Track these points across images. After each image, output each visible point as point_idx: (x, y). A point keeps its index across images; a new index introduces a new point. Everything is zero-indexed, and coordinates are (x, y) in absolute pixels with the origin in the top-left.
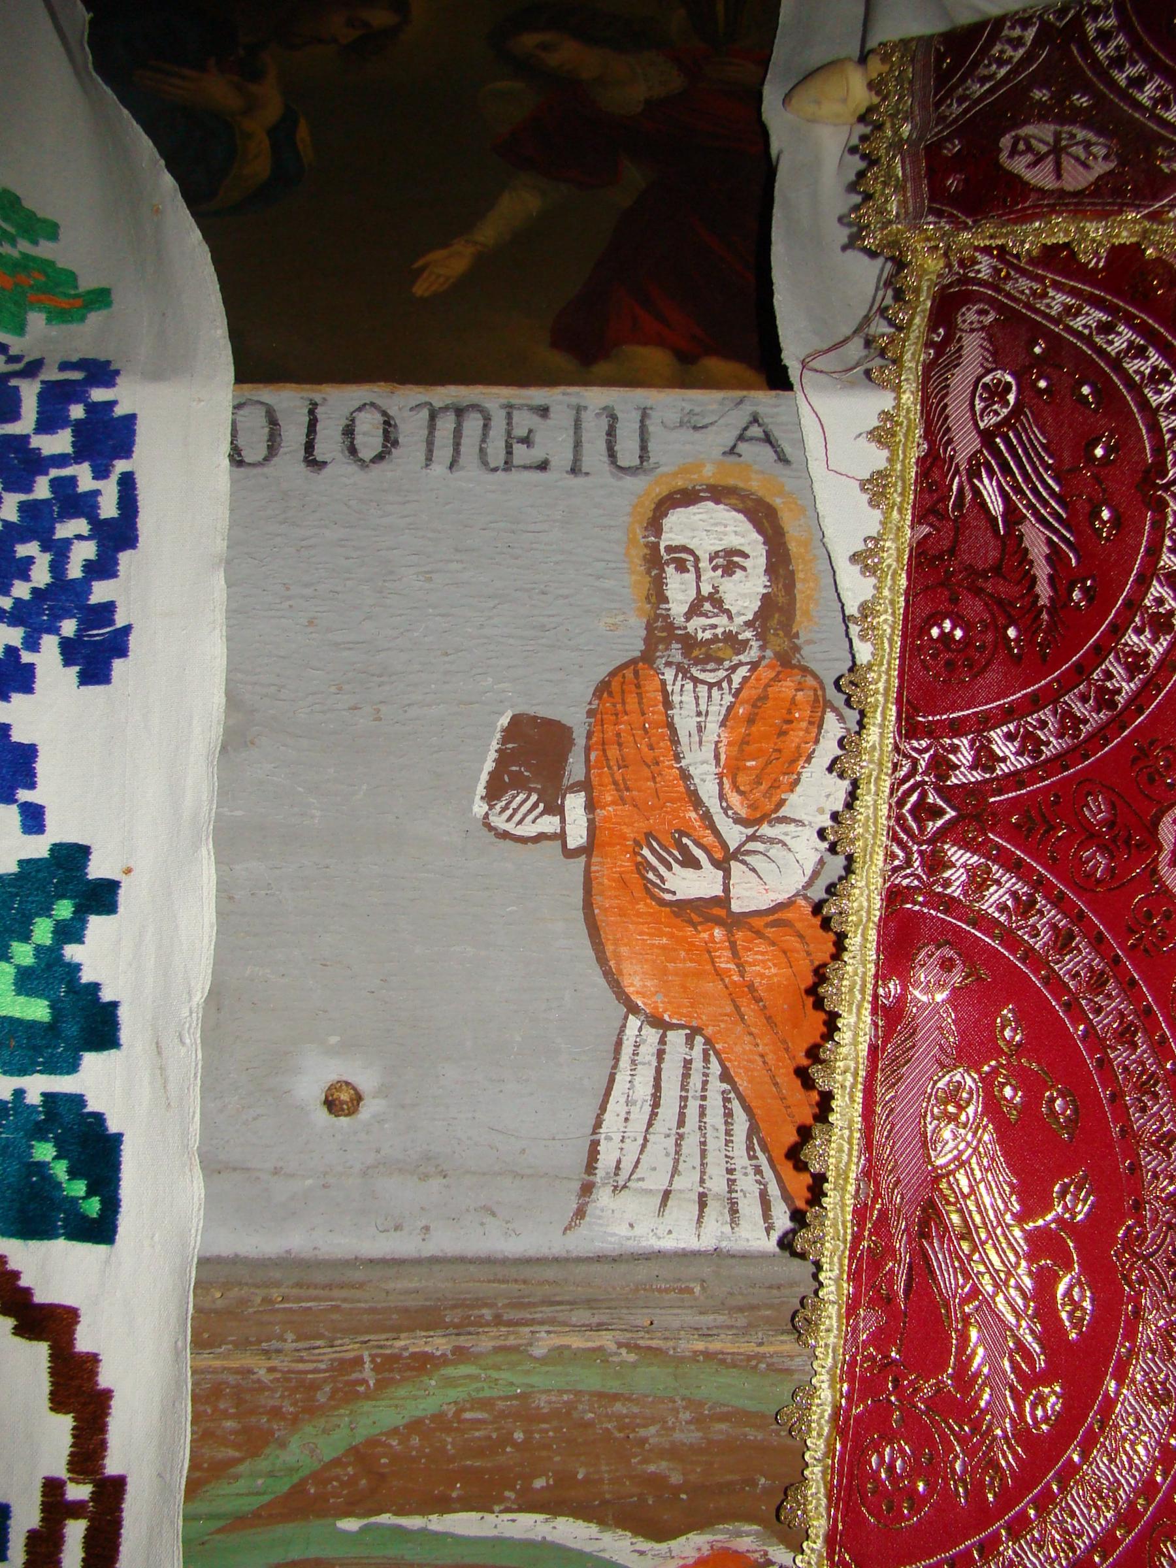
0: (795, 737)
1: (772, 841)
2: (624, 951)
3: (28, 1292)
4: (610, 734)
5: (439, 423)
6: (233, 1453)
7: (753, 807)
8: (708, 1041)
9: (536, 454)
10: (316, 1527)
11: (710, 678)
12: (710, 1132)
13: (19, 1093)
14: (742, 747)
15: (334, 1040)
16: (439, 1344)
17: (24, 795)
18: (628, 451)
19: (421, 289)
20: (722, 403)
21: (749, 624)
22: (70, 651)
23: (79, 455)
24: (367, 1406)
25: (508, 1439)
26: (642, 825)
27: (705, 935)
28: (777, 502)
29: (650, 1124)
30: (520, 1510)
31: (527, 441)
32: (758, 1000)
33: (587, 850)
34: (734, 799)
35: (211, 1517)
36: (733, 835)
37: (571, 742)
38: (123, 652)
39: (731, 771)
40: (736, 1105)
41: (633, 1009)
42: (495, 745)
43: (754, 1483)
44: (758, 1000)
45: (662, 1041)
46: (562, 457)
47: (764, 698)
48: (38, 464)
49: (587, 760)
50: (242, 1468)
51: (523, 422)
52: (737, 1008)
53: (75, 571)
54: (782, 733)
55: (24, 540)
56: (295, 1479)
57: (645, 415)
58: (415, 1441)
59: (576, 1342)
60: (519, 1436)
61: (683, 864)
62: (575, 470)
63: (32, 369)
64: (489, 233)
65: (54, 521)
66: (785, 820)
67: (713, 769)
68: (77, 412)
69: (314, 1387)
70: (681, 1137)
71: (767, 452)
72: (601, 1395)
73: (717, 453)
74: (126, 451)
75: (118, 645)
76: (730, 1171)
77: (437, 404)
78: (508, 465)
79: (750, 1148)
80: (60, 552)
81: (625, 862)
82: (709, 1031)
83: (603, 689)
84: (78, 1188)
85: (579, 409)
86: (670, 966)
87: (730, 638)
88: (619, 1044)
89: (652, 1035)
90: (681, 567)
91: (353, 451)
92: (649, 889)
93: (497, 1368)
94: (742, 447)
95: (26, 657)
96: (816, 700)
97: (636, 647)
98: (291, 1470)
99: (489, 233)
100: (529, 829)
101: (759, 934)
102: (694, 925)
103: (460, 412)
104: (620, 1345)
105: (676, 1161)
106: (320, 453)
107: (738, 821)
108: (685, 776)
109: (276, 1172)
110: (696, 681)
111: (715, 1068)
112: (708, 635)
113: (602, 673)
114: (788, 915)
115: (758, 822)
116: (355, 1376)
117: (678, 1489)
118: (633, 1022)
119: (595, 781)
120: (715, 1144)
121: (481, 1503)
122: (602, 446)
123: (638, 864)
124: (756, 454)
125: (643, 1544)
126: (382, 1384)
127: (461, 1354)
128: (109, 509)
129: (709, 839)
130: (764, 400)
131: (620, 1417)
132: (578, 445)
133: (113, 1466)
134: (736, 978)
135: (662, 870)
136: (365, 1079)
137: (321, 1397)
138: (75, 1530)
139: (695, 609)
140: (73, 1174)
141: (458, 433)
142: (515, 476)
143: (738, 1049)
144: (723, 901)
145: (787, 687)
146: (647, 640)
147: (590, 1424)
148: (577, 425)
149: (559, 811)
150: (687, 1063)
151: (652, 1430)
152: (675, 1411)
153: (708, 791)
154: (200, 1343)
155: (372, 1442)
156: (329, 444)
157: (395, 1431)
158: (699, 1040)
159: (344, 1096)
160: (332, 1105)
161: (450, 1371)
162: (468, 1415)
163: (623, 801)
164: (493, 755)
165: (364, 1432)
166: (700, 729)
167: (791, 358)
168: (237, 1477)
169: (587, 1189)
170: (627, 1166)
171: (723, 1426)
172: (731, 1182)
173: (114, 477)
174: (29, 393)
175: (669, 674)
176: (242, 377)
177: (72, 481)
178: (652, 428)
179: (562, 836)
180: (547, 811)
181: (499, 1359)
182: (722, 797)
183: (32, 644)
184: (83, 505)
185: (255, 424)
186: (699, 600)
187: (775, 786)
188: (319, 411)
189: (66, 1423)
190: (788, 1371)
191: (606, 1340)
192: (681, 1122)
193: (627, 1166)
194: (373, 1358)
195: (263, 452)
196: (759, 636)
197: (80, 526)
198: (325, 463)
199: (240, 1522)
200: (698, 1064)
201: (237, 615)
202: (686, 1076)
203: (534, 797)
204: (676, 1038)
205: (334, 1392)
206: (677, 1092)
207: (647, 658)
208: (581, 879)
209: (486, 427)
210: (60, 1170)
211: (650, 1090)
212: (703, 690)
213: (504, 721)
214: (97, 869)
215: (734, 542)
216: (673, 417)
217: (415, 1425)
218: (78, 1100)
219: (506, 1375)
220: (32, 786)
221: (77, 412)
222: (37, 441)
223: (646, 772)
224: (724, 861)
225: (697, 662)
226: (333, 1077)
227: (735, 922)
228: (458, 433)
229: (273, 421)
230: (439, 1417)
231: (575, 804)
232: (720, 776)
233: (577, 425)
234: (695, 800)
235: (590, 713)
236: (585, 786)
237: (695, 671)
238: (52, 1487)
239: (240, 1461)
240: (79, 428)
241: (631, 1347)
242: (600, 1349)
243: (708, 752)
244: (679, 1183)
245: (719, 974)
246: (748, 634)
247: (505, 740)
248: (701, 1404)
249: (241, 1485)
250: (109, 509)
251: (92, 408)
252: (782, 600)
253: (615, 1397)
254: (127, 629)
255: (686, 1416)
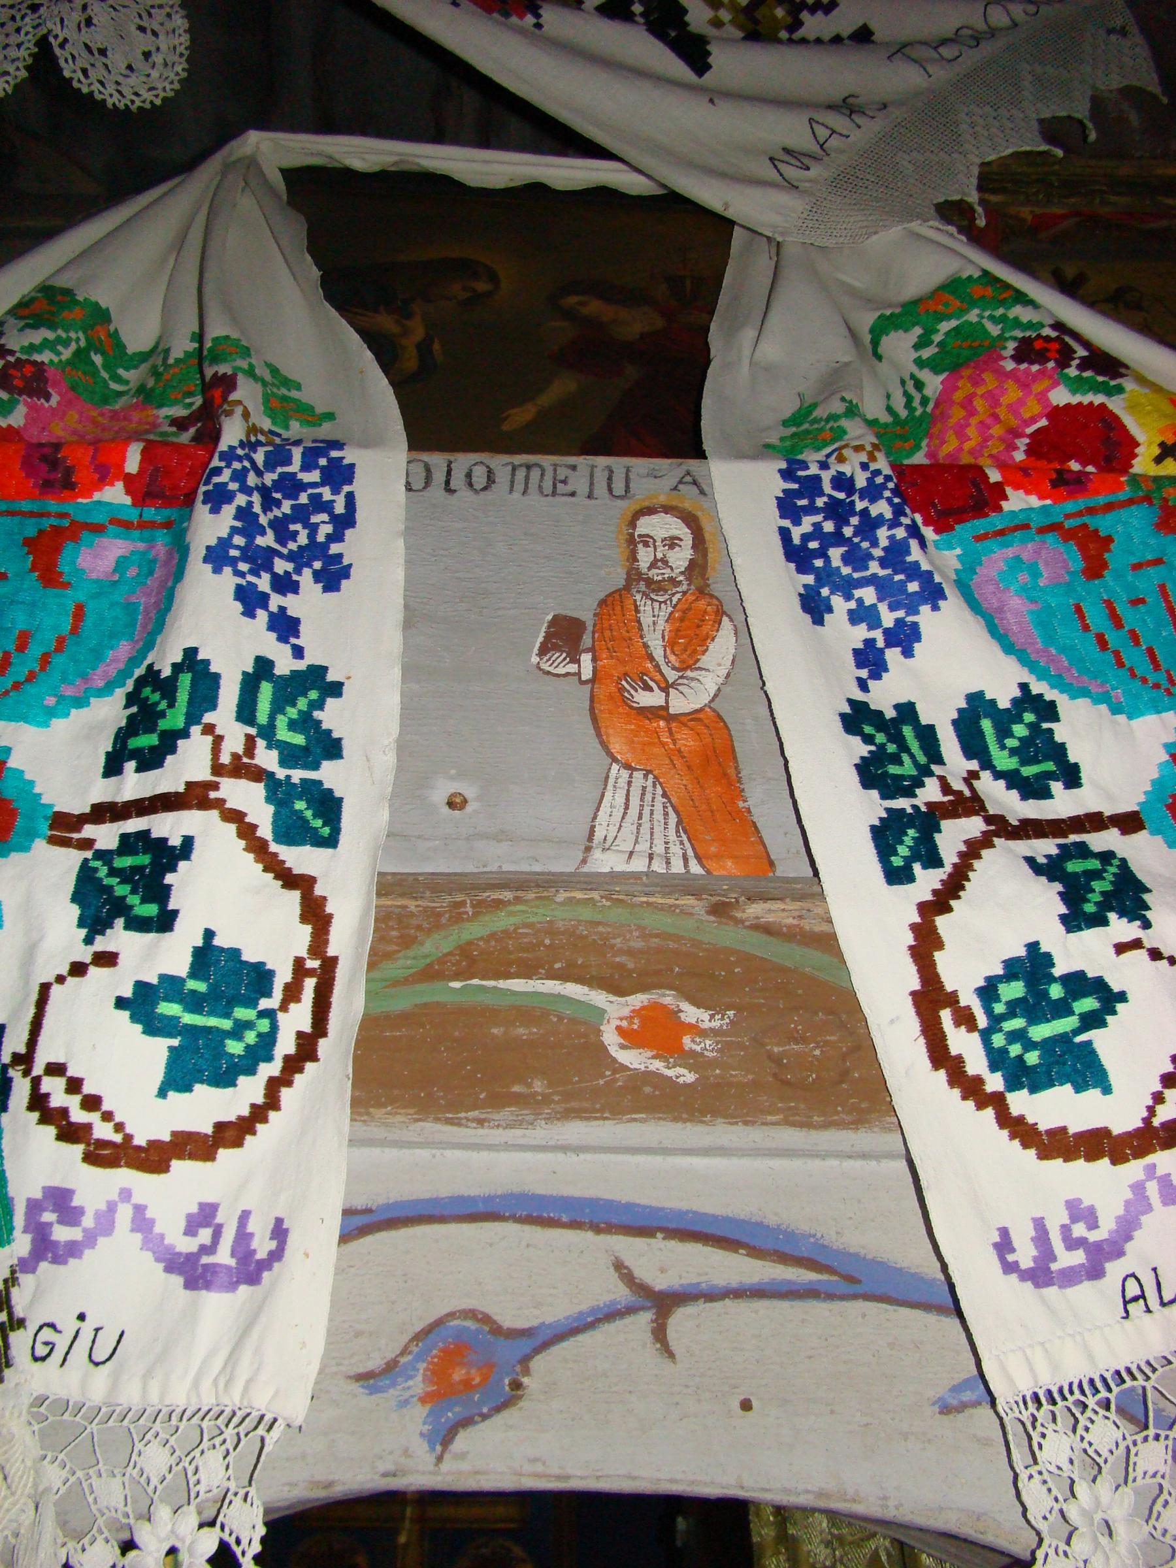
0: (706, 629)
1: (693, 679)
2: (611, 731)
3: (290, 869)
4: (606, 625)
5: (517, 473)
6: (395, 948)
7: (682, 662)
8: (655, 777)
9: (569, 488)
10: (438, 985)
11: (661, 599)
12: (656, 823)
13: (288, 777)
14: (677, 633)
15: (453, 772)
16: (507, 895)
17: (293, 641)
18: (619, 488)
19: (505, 427)
20: (670, 465)
21: (682, 573)
22: (317, 576)
23: (323, 484)
24: (467, 925)
25: (541, 943)
26: (622, 669)
27: (655, 725)
28: (699, 514)
29: (623, 818)
30: (547, 978)
31: (564, 482)
32: (683, 757)
33: (592, 681)
34: (672, 658)
35: (382, 980)
36: (671, 676)
37: (585, 628)
38: (347, 577)
39: (671, 644)
40: (670, 810)
41: (615, 760)
42: (544, 629)
43: (672, 970)
44: (683, 757)
45: (631, 776)
46: (582, 488)
47: (689, 609)
48: (302, 487)
49: (593, 638)
50: (401, 955)
51: (562, 473)
52: (672, 760)
53: (321, 538)
54: (698, 626)
55: (294, 523)
56: (428, 961)
57: (628, 471)
58: (493, 943)
59: (579, 895)
60: (547, 942)
61: (643, 689)
62: (590, 497)
63: (297, 443)
64: (546, 399)
65: (310, 514)
66: (700, 669)
67: (661, 643)
68: (323, 462)
69: (440, 915)
70: (640, 825)
71: (695, 490)
72: (591, 922)
73: (667, 489)
74: (350, 482)
75: (345, 573)
76: (666, 843)
77: (516, 463)
78: (554, 494)
79: (677, 831)
80: (313, 529)
81: (613, 689)
82: (656, 772)
83: (603, 603)
84: (318, 823)
85: (593, 467)
86: (636, 739)
87: (672, 580)
88: (607, 777)
89: (625, 774)
90: (646, 545)
91: (471, 485)
92: (625, 702)
93: (538, 907)
94: (681, 487)
95: (295, 577)
96: (718, 610)
97: (621, 583)
98: (426, 956)
99: (546, 399)
100: (561, 670)
101: (685, 725)
102: (649, 719)
103: (529, 467)
104: (602, 897)
105: (637, 837)
106: (453, 485)
107: (674, 668)
108: (646, 646)
109: (419, 837)
110: (652, 600)
111: (659, 791)
112: (660, 578)
113: (602, 595)
114: (701, 716)
115: (685, 669)
116: (462, 910)
117: (633, 971)
118: (615, 767)
119: (597, 648)
120: (659, 829)
121: (528, 972)
122: (605, 485)
123: (619, 689)
124: (689, 491)
125: (612, 998)
126: (476, 914)
127: (518, 900)
128: (340, 508)
129: (658, 677)
130: (693, 464)
131: (601, 933)
132: (592, 484)
133: (331, 951)
134: (672, 746)
135: (632, 692)
136: (470, 792)
137: (444, 920)
138: (310, 984)
139: (653, 565)
140: (315, 816)
141: (527, 478)
142: (558, 499)
143: (672, 782)
144: (666, 708)
145: (702, 604)
146: (626, 580)
147: (586, 937)
148: (592, 476)
149: (578, 662)
150: (644, 788)
151: (618, 940)
152: (631, 932)
153: (658, 654)
154: (379, 894)
155: (470, 943)
156: (458, 481)
157: (482, 938)
158: (651, 776)
159: (458, 800)
160: (451, 804)
161: (511, 908)
162: (521, 931)
163: (612, 657)
164: (542, 634)
165: (466, 936)
166: (654, 623)
167: (706, 446)
168: (398, 959)
169: (588, 849)
170: (610, 839)
171: (656, 940)
172: (667, 849)
173: (343, 494)
174: (297, 454)
175: (638, 597)
176: (410, 450)
177: (320, 495)
178: (632, 476)
179: (579, 674)
180: (571, 662)
181: (538, 903)
182: (665, 657)
183: (298, 571)
184: (327, 507)
185: (419, 471)
186: (656, 560)
187: (695, 651)
188: (453, 465)
189: (308, 929)
190: (691, 914)
191: (595, 895)
192: (640, 818)
193: (610, 839)
194: (471, 901)
195: (421, 485)
196: (687, 579)
197: (324, 517)
198: (455, 491)
199: (396, 983)
200: (650, 789)
201: (409, 563)
202: (643, 794)
203: (564, 655)
204: (638, 775)
205: (451, 917)
206: (638, 802)
207: (627, 588)
208: (588, 695)
209: (542, 475)
210: (309, 814)
211: (623, 801)
212: (656, 605)
213: (550, 617)
214: (331, 677)
215: (676, 533)
216: (644, 471)
217: (492, 935)
218: (320, 783)
219: (541, 911)
220: (298, 637)
221: (323, 462)
222: (300, 476)
223: (625, 644)
224: (666, 688)
225: (653, 591)
226: (453, 791)
227: (671, 718)
228: (527, 478)
229: (428, 470)
230: (505, 932)
231: (586, 659)
232: (665, 647)
233: (592, 476)
234: (651, 658)
235: (595, 615)
236: (592, 650)
237: (653, 596)
238: (299, 962)
239: (398, 951)
240: (323, 470)
241: (608, 899)
242: (592, 899)
243: (658, 634)
244: (638, 848)
245: (663, 744)
246: (681, 578)
247: (549, 627)
248: (644, 928)
249: (401, 963)
250: (340, 508)
251: (330, 460)
252: (700, 562)
253: (599, 923)
254: (350, 566)
255: (636, 934)
